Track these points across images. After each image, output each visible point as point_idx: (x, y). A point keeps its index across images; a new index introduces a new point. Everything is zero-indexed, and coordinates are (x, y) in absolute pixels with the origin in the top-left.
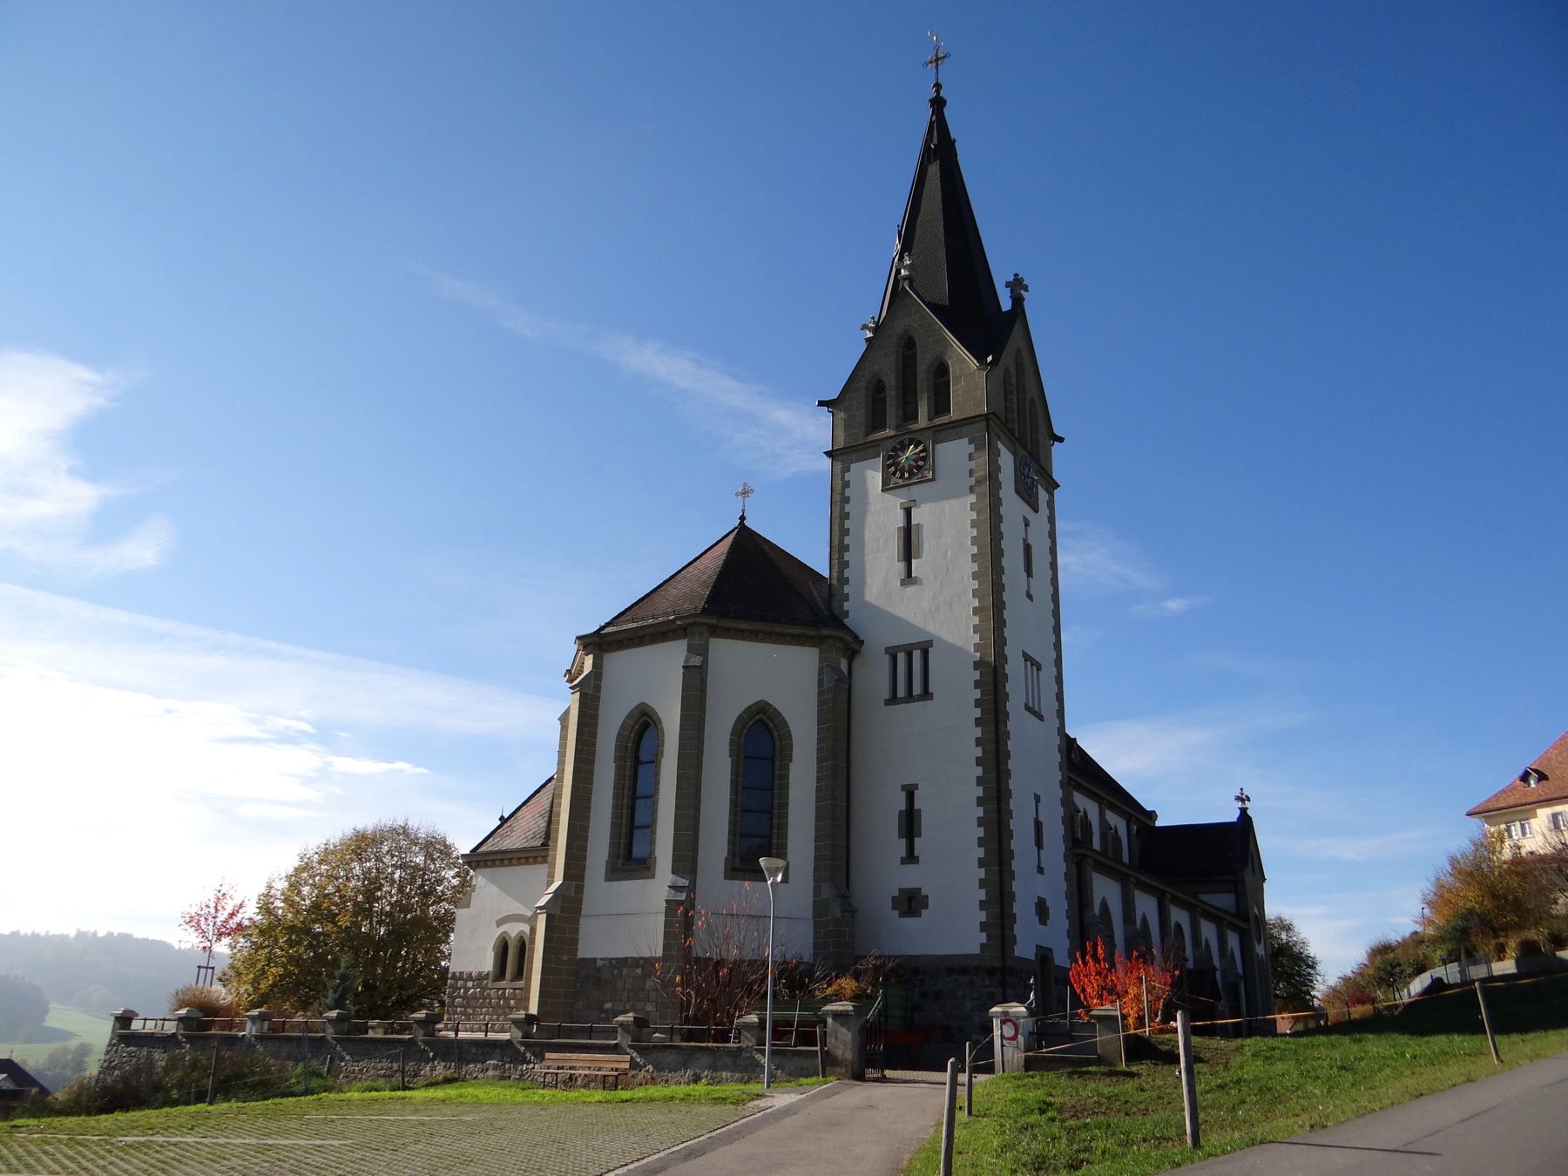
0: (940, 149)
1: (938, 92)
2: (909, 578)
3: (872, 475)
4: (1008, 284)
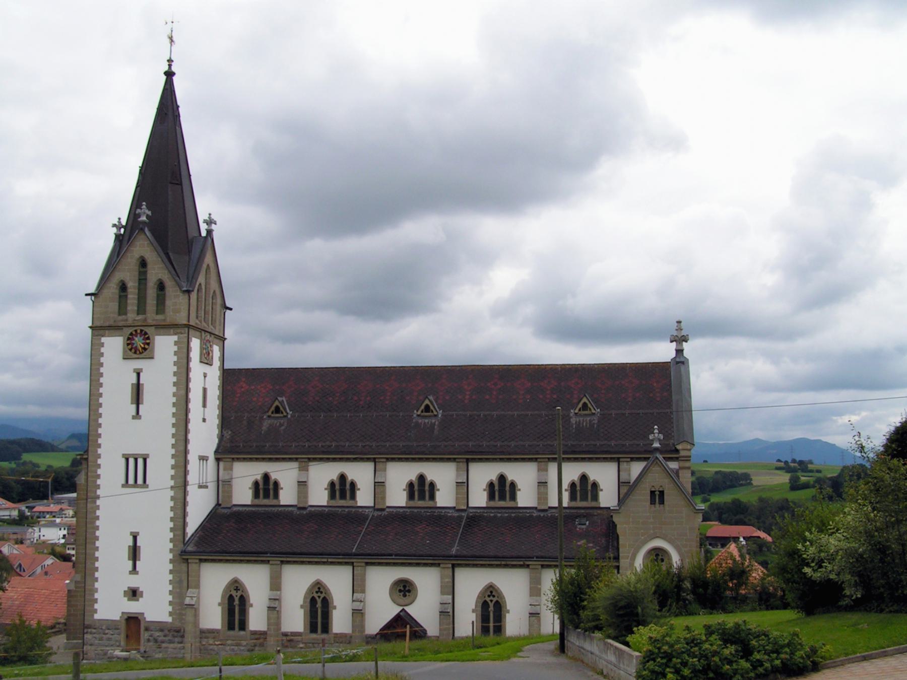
0: (168, 110)
1: (170, 66)
2: (137, 415)
3: (114, 345)
4: (205, 221)
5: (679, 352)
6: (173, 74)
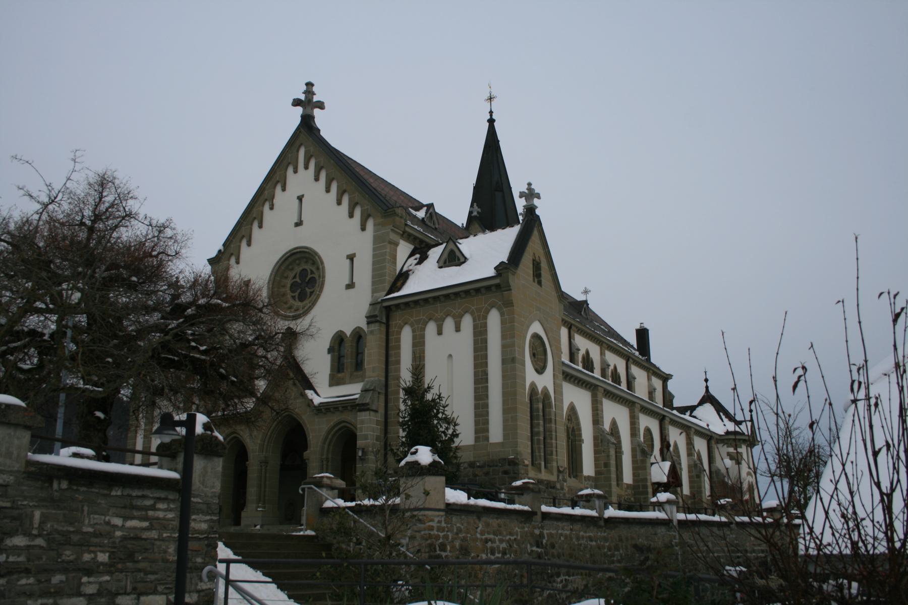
0: (492, 146)
1: (491, 115)
4: (522, 195)
5: (85, 595)
6: (494, 121)
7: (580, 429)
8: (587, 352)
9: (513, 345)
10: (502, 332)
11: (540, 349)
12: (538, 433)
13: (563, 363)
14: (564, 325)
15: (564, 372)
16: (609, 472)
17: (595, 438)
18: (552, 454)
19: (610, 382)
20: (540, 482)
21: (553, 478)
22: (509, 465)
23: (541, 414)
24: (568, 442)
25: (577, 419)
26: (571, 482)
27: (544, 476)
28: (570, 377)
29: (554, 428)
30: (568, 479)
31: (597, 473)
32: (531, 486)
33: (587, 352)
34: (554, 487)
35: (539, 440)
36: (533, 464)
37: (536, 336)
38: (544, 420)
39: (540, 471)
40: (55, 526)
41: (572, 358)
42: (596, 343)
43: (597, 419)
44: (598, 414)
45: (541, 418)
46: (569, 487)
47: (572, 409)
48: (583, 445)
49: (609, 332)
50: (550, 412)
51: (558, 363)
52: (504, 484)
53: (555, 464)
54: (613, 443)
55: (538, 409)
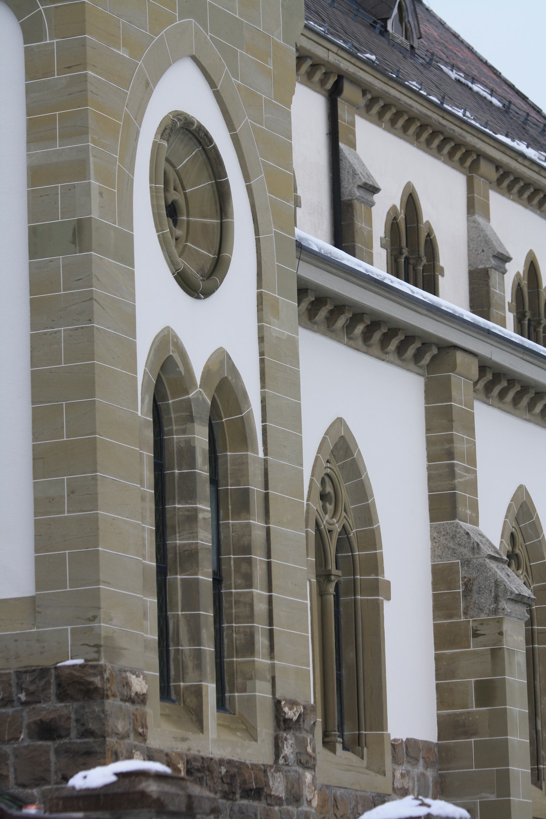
7: (372, 539)
8: (411, 201)
9: (79, 168)
10: (31, 109)
11: (200, 187)
12: (191, 556)
13: (301, 248)
14: (308, 79)
15: (303, 290)
16: (500, 723)
17: (441, 576)
18: (249, 647)
19: (509, 331)
20: (199, 769)
21: (256, 752)
22: (62, 696)
23: (203, 470)
24: (322, 594)
25: (362, 491)
26: (336, 768)
27: (216, 742)
28: (322, 309)
29: (258, 535)
30: (322, 754)
31: (447, 726)
32: (153, 788)
33: (411, 201)
34: (257, 793)
35: (191, 587)
36: (165, 692)
37: (184, 131)
38: (217, 501)
39: (199, 723)
40: (66, 740)
41: (344, 227)
42: (449, 159)
43: (448, 499)
44: (451, 472)
45: (204, 488)
46: (324, 790)
47: (341, 449)
48: (389, 610)
49: (507, 109)
50: (243, 463)
51: (281, 248)
52: (40, 781)
53: (262, 692)
54: (519, 599)
55: (188, 452)
